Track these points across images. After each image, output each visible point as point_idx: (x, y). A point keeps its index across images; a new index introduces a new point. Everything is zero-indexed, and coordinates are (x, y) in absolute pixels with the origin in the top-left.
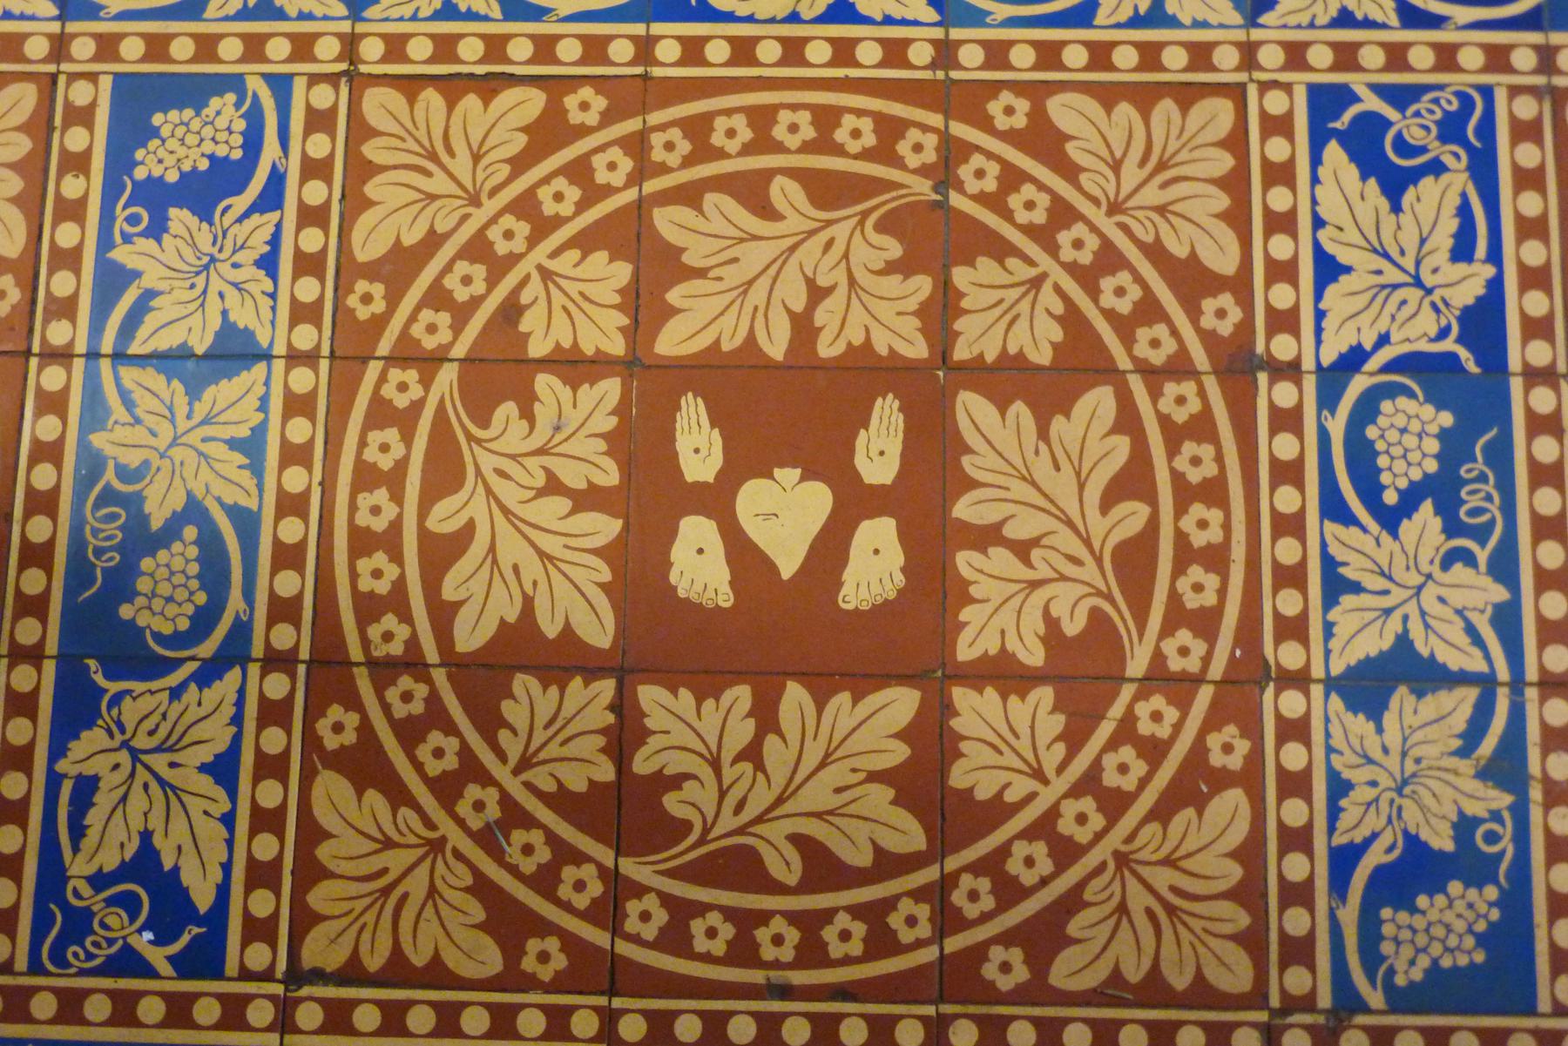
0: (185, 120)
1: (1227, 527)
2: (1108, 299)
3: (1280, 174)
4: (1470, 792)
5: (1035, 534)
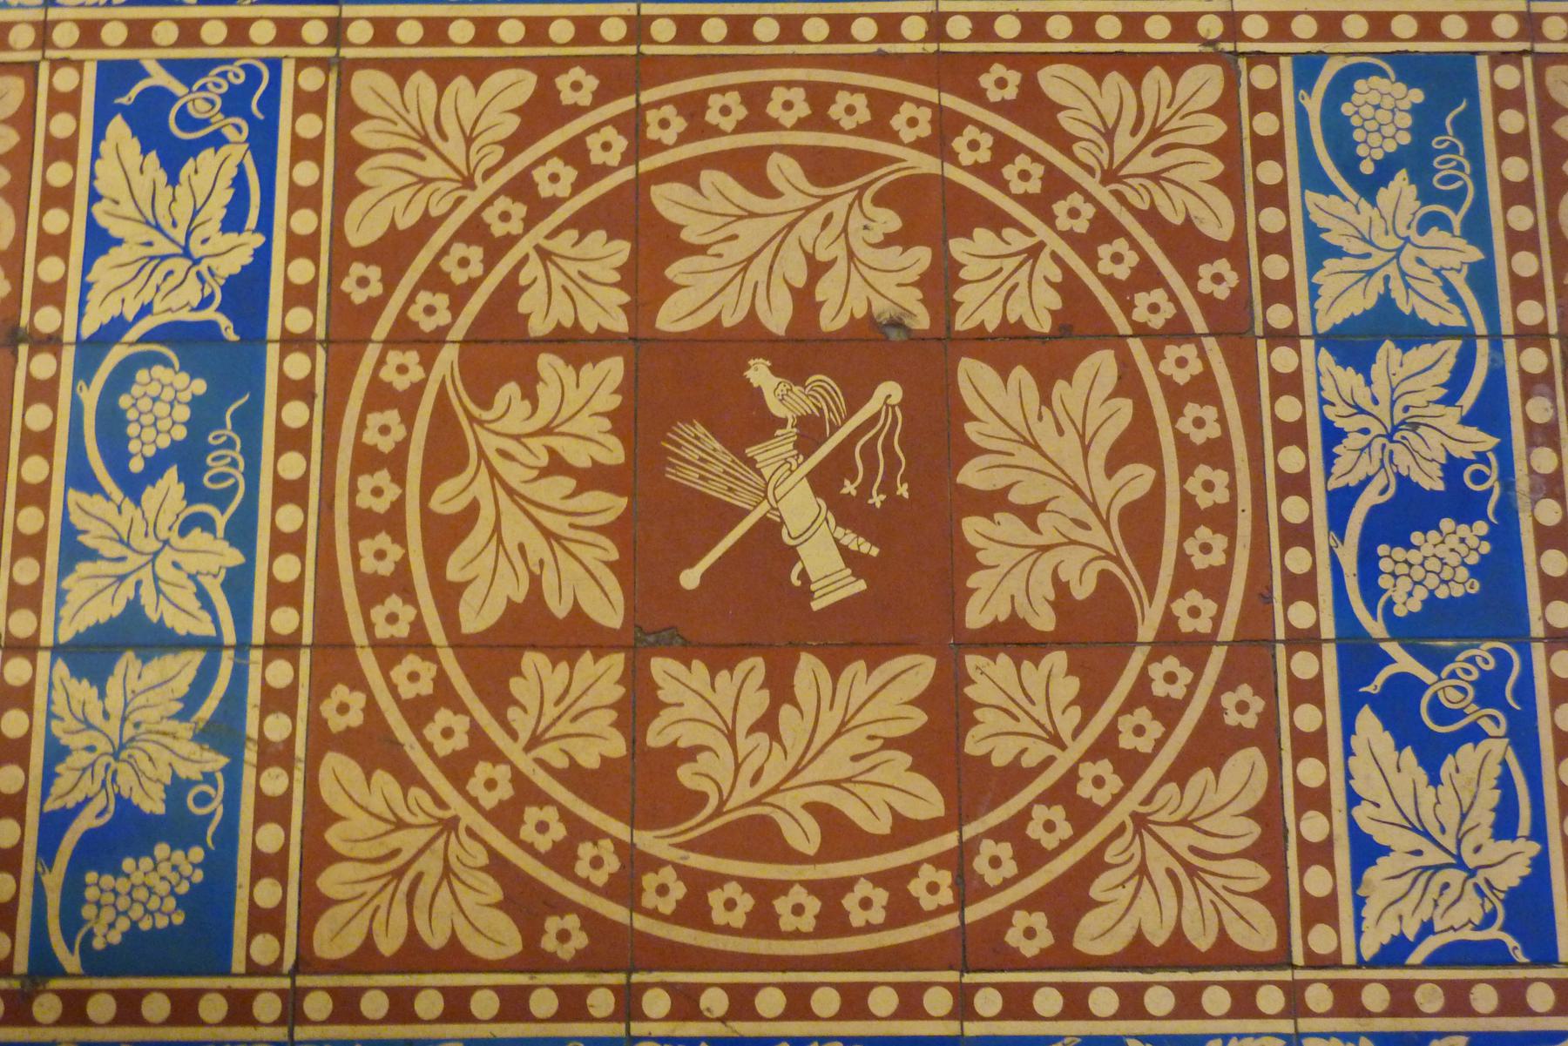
0: (1444, 587)
1: (1232, 486)
2: (1105, 267)
3: (62, 150)
4: (186, 755)
5: (544, 482)
